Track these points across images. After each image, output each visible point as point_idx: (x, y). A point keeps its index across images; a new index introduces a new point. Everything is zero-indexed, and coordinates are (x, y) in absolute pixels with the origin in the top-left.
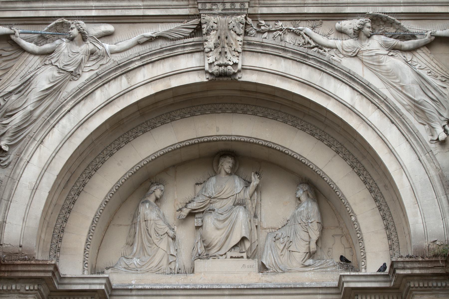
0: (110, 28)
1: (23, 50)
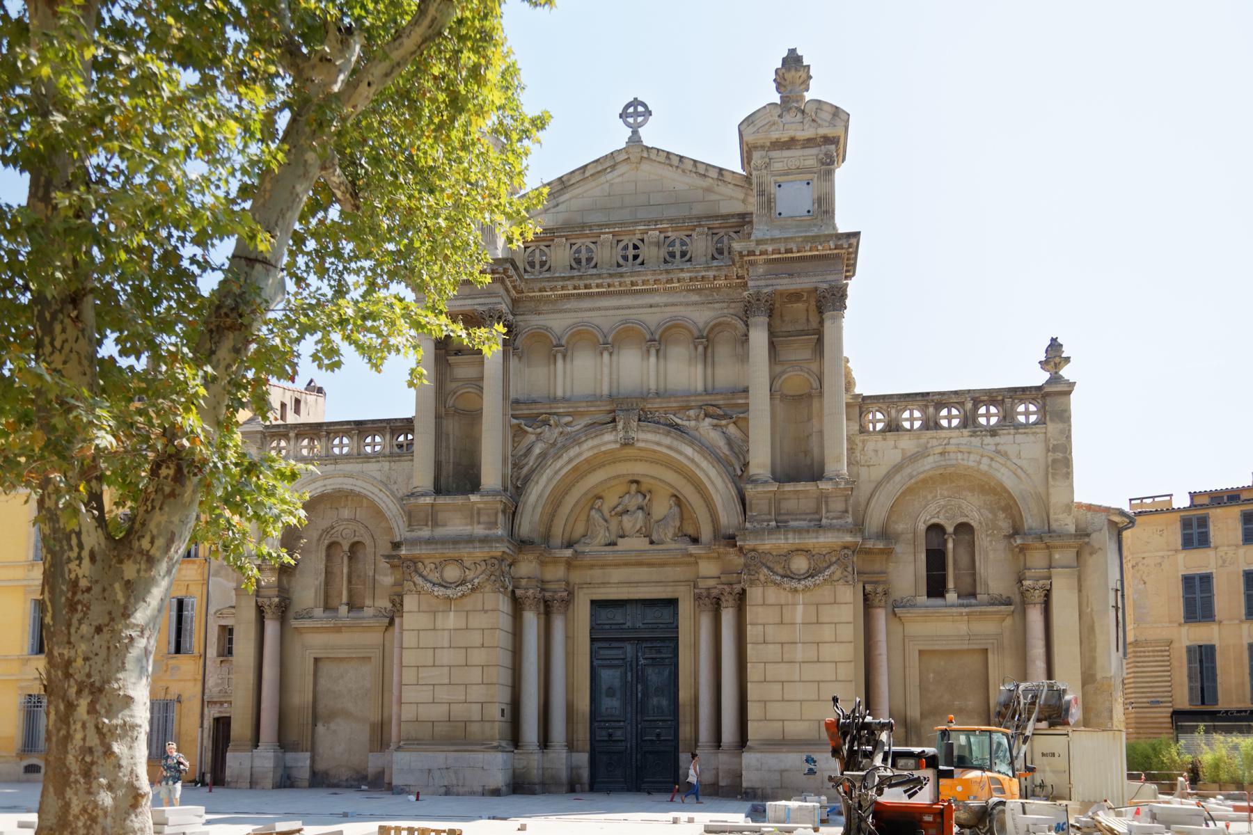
0: (570, 419)
1: (526, 432)
